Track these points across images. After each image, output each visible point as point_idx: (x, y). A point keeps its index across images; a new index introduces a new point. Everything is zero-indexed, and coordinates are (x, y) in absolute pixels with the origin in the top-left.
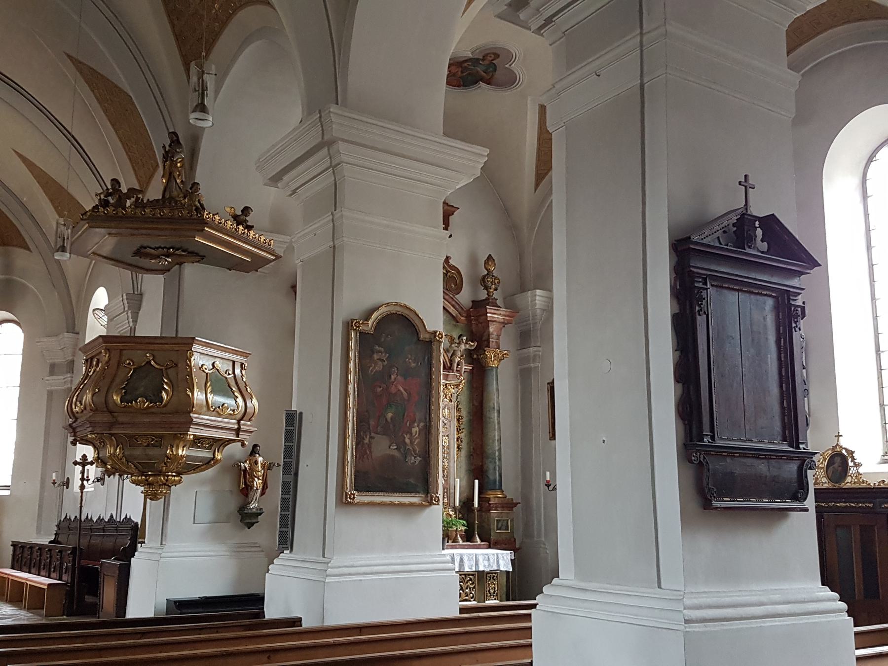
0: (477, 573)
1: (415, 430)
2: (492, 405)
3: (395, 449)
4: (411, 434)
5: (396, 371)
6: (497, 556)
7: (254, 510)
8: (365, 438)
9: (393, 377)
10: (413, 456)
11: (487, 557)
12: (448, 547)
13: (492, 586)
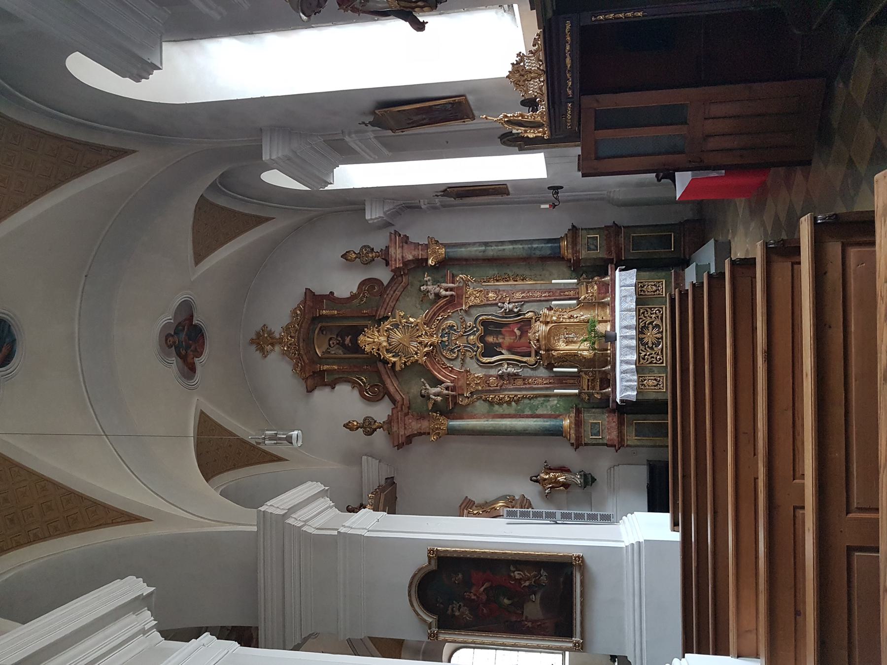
0: (637, 307)
1: (517, 575)
2: (481, 254)
3: (535, 597)
4: (521, 579)
5: (468, 594)
6: (622, 286)
7: (582, 481)
8: (527, 626)
9: (473, 597)
10: (540, 577)
11: (623, 298)
12: (614, 315)
13: (650, 288)
